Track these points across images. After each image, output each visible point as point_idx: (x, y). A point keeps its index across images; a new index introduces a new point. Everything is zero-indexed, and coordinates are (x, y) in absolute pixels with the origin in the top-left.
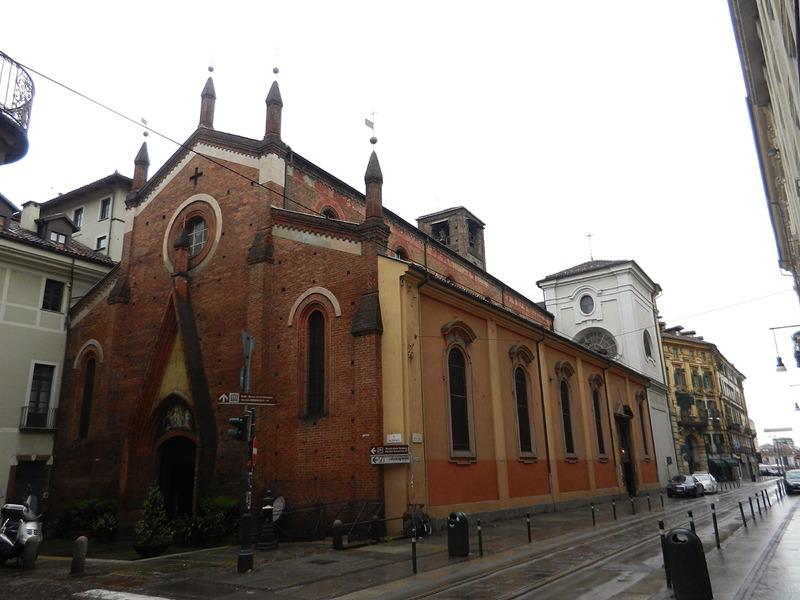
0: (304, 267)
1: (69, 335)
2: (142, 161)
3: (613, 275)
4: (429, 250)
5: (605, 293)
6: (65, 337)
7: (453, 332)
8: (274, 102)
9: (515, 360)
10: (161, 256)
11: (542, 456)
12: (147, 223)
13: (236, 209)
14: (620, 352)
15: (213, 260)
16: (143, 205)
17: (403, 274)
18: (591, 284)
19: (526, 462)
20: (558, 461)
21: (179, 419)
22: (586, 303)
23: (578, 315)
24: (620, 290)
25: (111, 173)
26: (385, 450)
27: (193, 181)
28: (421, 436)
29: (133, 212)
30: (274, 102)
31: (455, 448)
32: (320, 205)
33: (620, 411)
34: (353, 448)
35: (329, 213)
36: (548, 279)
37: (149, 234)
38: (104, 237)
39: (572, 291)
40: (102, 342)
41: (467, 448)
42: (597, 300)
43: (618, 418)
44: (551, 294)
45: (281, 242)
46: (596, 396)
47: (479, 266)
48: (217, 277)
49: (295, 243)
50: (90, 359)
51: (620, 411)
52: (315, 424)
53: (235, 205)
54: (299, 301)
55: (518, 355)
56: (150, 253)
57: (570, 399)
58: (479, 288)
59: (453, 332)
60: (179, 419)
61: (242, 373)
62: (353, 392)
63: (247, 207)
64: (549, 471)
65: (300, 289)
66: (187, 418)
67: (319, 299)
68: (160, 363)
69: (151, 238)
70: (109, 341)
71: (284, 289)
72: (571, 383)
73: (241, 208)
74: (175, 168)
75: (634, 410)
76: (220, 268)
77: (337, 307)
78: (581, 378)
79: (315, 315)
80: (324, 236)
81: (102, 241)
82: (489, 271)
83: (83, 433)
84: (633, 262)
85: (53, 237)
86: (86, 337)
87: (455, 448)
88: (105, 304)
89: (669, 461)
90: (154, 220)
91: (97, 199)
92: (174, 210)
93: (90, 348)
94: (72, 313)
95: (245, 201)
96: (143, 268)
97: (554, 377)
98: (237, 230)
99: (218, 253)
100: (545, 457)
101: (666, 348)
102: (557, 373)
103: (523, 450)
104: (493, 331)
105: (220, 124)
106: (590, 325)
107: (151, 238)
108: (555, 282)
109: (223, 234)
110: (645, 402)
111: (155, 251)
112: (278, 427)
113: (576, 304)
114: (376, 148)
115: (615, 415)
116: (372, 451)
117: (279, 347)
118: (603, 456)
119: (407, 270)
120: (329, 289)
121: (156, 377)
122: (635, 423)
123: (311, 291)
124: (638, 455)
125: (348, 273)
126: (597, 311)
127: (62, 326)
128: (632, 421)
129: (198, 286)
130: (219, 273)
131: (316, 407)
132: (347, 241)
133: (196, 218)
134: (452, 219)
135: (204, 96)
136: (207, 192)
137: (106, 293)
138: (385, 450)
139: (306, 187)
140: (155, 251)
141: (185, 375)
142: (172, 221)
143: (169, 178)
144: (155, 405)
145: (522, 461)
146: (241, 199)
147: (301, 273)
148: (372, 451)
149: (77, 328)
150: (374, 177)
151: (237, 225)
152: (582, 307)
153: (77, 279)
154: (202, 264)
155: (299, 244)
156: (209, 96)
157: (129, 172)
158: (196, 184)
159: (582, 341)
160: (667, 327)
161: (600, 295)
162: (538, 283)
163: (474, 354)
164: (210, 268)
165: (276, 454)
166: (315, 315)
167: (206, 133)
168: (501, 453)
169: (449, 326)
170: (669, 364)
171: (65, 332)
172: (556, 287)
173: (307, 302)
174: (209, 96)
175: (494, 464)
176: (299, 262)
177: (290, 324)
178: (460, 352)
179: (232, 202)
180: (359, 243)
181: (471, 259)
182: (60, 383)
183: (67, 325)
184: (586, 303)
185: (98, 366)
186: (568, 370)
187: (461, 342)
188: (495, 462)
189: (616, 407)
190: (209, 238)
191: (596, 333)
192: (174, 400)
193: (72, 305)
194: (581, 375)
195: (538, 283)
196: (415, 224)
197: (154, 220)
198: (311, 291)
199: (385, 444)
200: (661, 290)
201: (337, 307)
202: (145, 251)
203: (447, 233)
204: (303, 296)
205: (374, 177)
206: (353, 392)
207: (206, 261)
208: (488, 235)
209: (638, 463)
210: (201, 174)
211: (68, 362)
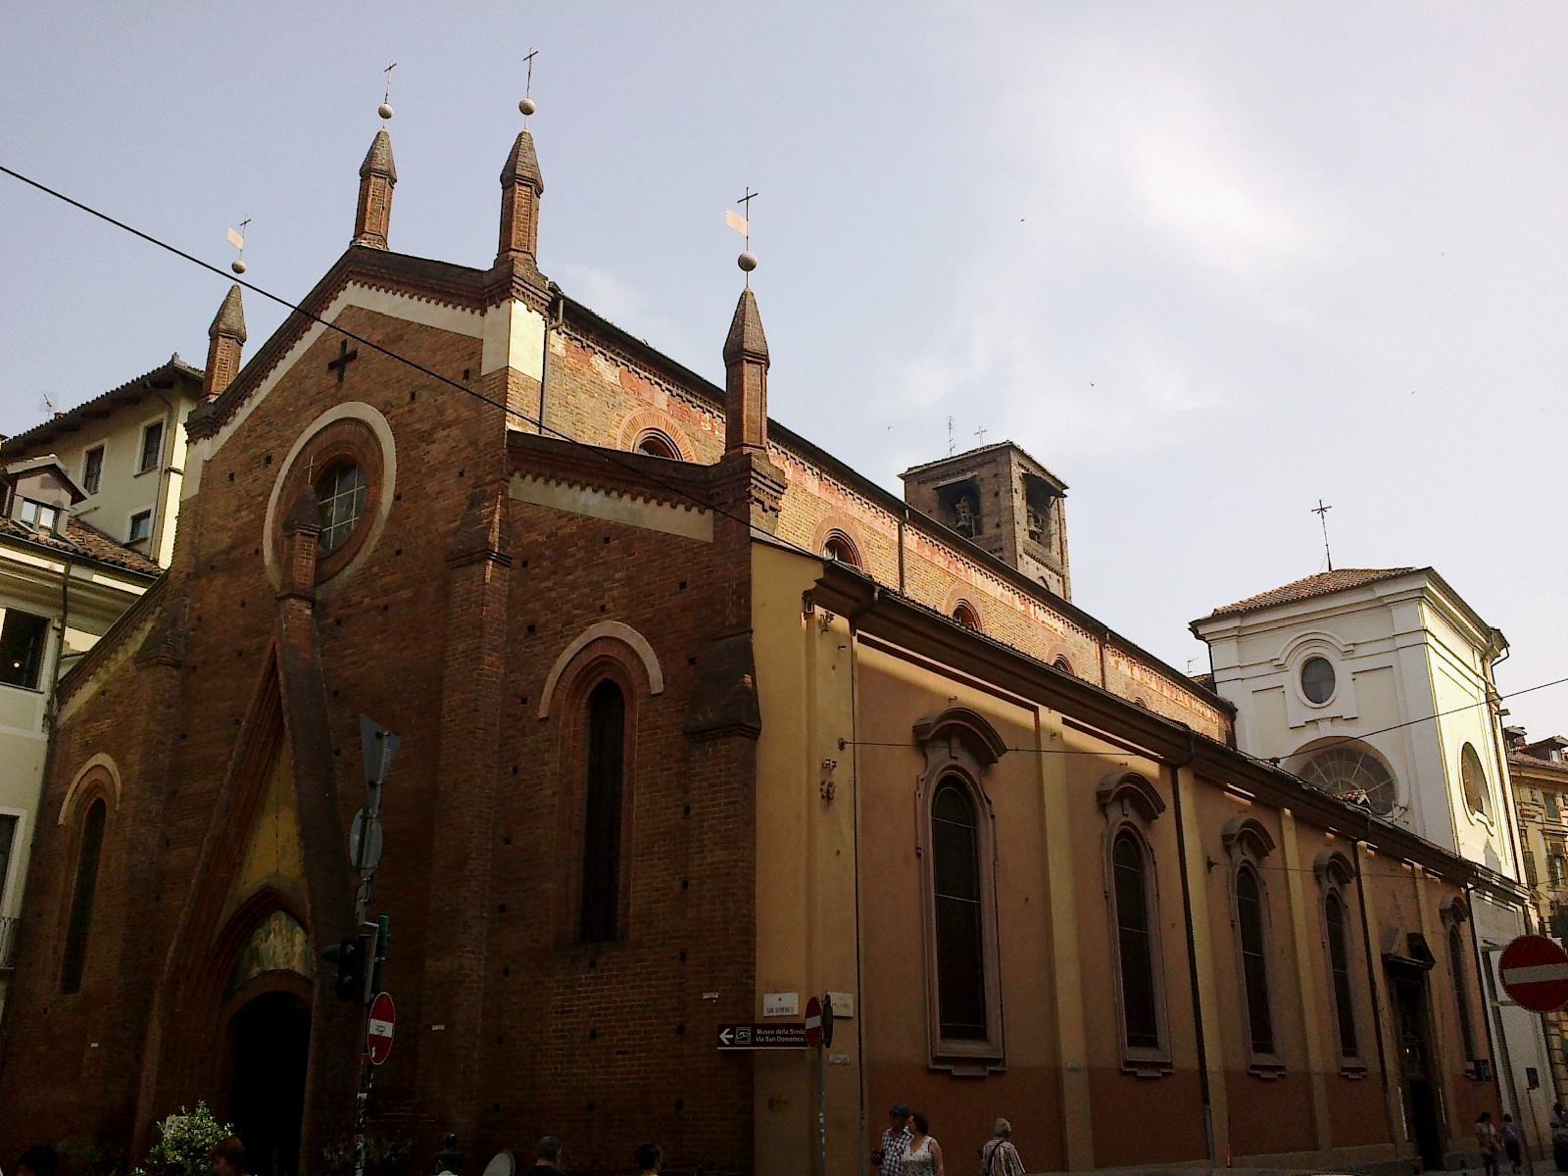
0: (579, 572)
1: (52, 743)
2: (224, 331)
3: (1383, 605)
4: (911, 539)
5: (1361, 651)
6: (43, 748)
7: (1121, 796)
8: (519, 181)
9: (1236, 852)
10: (258, 552)
11: (1185, 1061)
12: (232, 476)
13: (427, 437)
14: (1402, 801)
15: (371, 563)
16: (226, 433)
17: (812, 585)
18: (1324, 629)
19: (1141, 1073)
20: (1229, 1075)
21: (284, 947)
22: (1317, 679)
23: (1299, 708)
24: (1400, 642)
25: (163, 361)
26: (754, 1034)
27: (336, 372)
28: (850, 999)
29: (207, 448)
30: (519, 181)
31: (947, 1034)
32: (633, 424)
33: (1400, 949)
34: (681, 1030)
35: (656, 444)
36: (1218, 616)
37: (234, 503)
38: (147, 514)
39: (1282, 646)
40: (120, 761)
41: (979, 1033)
42: (1342, 670)
43: (1391, 965)
44: (1228, 653)
45: (528, 513)
46: (1333, 908)
47: (1055, 588)
48: (382, 601)
49: (561, 515)
50: (95, 810)
51: (1400, 949)
52: (593, 965)
53: (426, 426)
54: (567, 655)
55: (1240, 840)
56: (233, 547)
57: (1264, 913)
58: (1039, 635)
59: (1121, 796)
60: (284, 947)
61: (357, 822)
62: (685, 885)
63: (455, 432)
64: (1206, 1100)
65: (570, 627)
66: (298, 949)
67: (613, 652)
68: (244, 816)
69: (238, 510)
70: (133, 756)
71: (531, 629)
72: (1263, 873)
73: (441, 434)
74: (298, 344)
75: (1436, 943)
76: (388, 579)
77: (655, 672)
78: (1293, 861)
79: (604, 692)
80: (627, 498)
81: (143, 522)
82: (1077, 602)
83: (70, 983)
84: (1429, 571)
85: (27, 512)
86: (89, 750)
87: (947, 1034)
88: (132, 668)
89: (1532, 1073)
90: (248, 467)
91: (137, 423)
92: (291, 442)
93: (94, 776)
94: (62, 690)
95: (450, 414)
96: (219, 582)
97: (1218, 854)
98: (432, 487)
99: (385, 539)
100: (1379, 1070)
101: (1525, 794)
102: (1227, 848)
103: (1132, 1042)
104: (1185, 788)
105: (405, 238)
106: (1327, 730)
107: (238, 510)
108: (1237, 623)
109: (397, 497)
110: (1465, 926)
111: (246, 541)
112: (506, 973)
113: (1292, 679)
114: (755, 280)
115: (1384, 957)
116: (724, 1036)
117: (515, 770)
118: (1351, 1062)
119: (821, 575)
120: (636, 626)
121: (231, 849)
122: (1439, 978)
123: (596, 631)
124: (1450, 1060)
125: (683, 585)
126: (1345, 697)
127: (39, 721)
128: (1432, 973)
129: (338, 622)
130: (385, 592)
131: (599, 914)
132: (667, 505)
133: (340, 463)
134: (985, 472)
135: (367, 172)
136: (366, 397)
137: (135, 643)
138: (754, 1034)
139: (598, 383)
140: (246, 541)
141: (295, 840)
142: (284, 472)
143: (283, 367)
144: (228, 911)
145: (1130, 1070)
146: (441, 412)
147: (573, 587)
148: (724, 1036)
149: (69, 729)
150: (743, 351)
151: (432, 473)
152: (388, 118)
153: (76, 612)
154: (349, 571)
155: (571, 517)
156: (376, 174)
157: (195, 359)
158: (341, 378)
159: (1307, 769)
160: (1529, 740)
161: (1348, 653)
162: (1195, 627)
163: (1161, 836)
164: (365, 579)
165: (500, 1040)
166: (604, 692)
167: (367, 263)
168: (1072, 1051)
169: (1111, 787)
170: (1533, 830)
171: (45, 737)
172: (1239, 635)
173: (586, 659)
174: (376, 174)
175: (1053, 1076)
176: (568, 562)
177: (542, 714)
178: (1134, 840)
179: (421, 420)
180: (709, 513)
181: (1030, 569)
182: (26, 859)
183: (50, 720)
184: (1317, 679)
185: (110, 815)
186: (1254, 840)
187: (965, 761)
188: (1057, 1071)
189: (1388, 937)
190: (369, 509)
191: (1346, 754)
192: (268, 902)
193: (63, 673)
194: (1296, 853)
195: (1195, 627)
196: (897, 489)
197: (248, 467)
198: (596, 631)
199: (758, 1021)
200: (1505, 644)
201: (655, 672)
202: (225, 540)
203: (976, 509)
204: (576, 645)
205: (743, 351)
206: (685, 885)
207: (360, 561)
208: (1072, 507)
209: (1447, 1077)
210: (354, 355)
211: (48, 805)
